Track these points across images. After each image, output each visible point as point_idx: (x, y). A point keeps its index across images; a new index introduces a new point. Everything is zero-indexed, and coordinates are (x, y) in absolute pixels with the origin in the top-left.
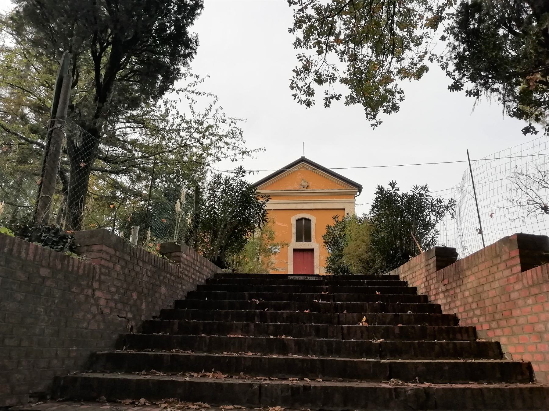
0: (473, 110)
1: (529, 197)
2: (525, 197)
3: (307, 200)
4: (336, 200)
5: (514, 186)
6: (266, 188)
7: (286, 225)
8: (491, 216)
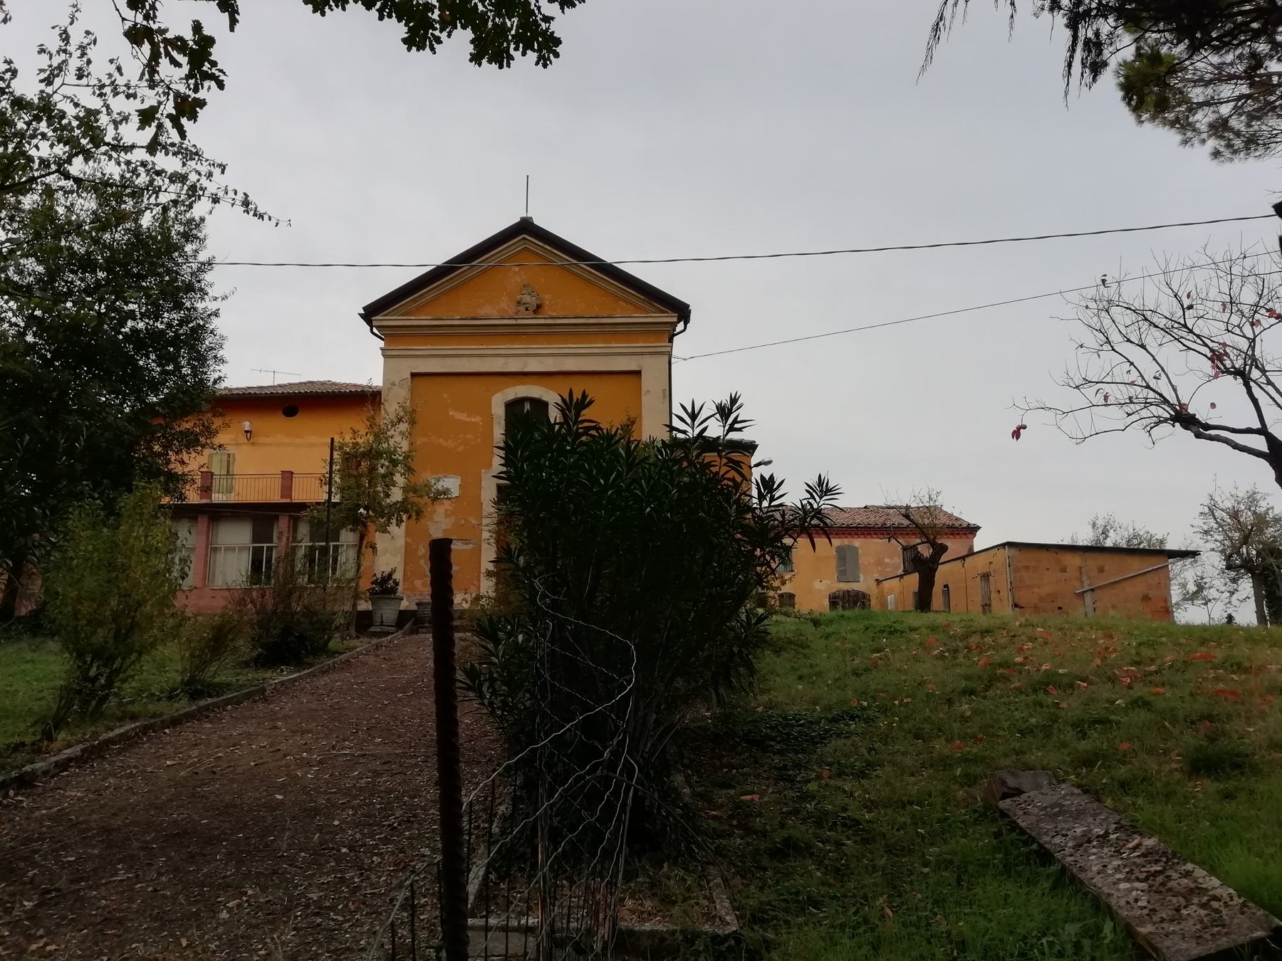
0: (929, 57)
1: (1134, 376)
2: (1121, 372)
3: (535, 348)
4: (616, 346)
5: (1093, 340)
6: (418, 310)
7: (477, 419)
8: (1016, 434)
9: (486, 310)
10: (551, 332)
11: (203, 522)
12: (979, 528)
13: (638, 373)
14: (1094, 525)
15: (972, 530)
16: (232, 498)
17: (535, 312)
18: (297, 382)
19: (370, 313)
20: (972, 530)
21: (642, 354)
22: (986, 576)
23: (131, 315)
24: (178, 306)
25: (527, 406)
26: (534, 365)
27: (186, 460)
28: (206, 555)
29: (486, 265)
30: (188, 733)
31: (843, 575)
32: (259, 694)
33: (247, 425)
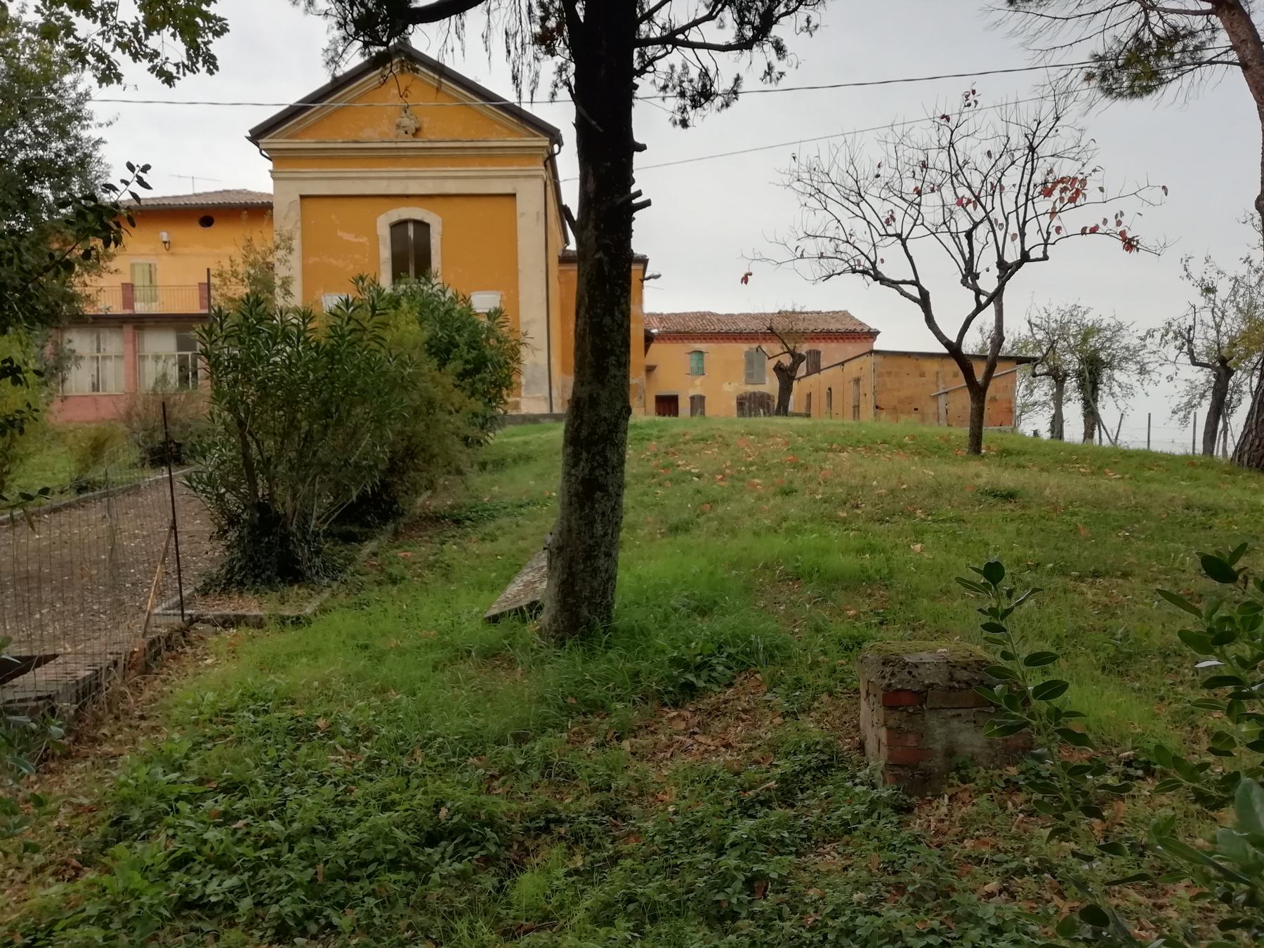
3: (415, 171)
7: (364, 240)
8: (745, 279)
9: (368, 133)
10: (430, 155)
11: (128, 329)
12: (878, 332)
13: (514, 195)
14: (981, 330)
15: (873, 335)
16: (155, 309)
17: (414, 135)
18: (212, 190)
19: (257, 135)
20: (873, 335)
21: (516, 177)
22: (857, 381)
23: (21, 144)
24: (64, 134)
25: (411, 228)
26: (414, 188)
27: (88, 282)
28: (135, 362)
29: (336, 105)
30: (63, 517)
31: (750, 378)
32: (135, 489)
33: (164, 236)
